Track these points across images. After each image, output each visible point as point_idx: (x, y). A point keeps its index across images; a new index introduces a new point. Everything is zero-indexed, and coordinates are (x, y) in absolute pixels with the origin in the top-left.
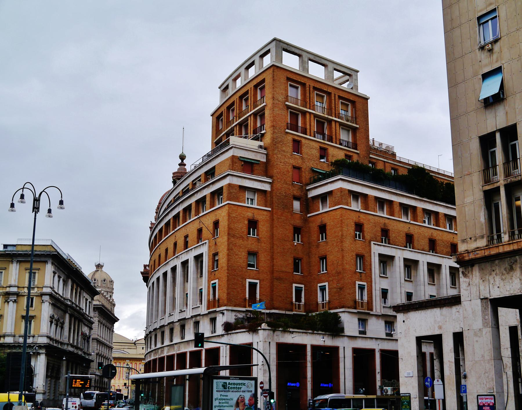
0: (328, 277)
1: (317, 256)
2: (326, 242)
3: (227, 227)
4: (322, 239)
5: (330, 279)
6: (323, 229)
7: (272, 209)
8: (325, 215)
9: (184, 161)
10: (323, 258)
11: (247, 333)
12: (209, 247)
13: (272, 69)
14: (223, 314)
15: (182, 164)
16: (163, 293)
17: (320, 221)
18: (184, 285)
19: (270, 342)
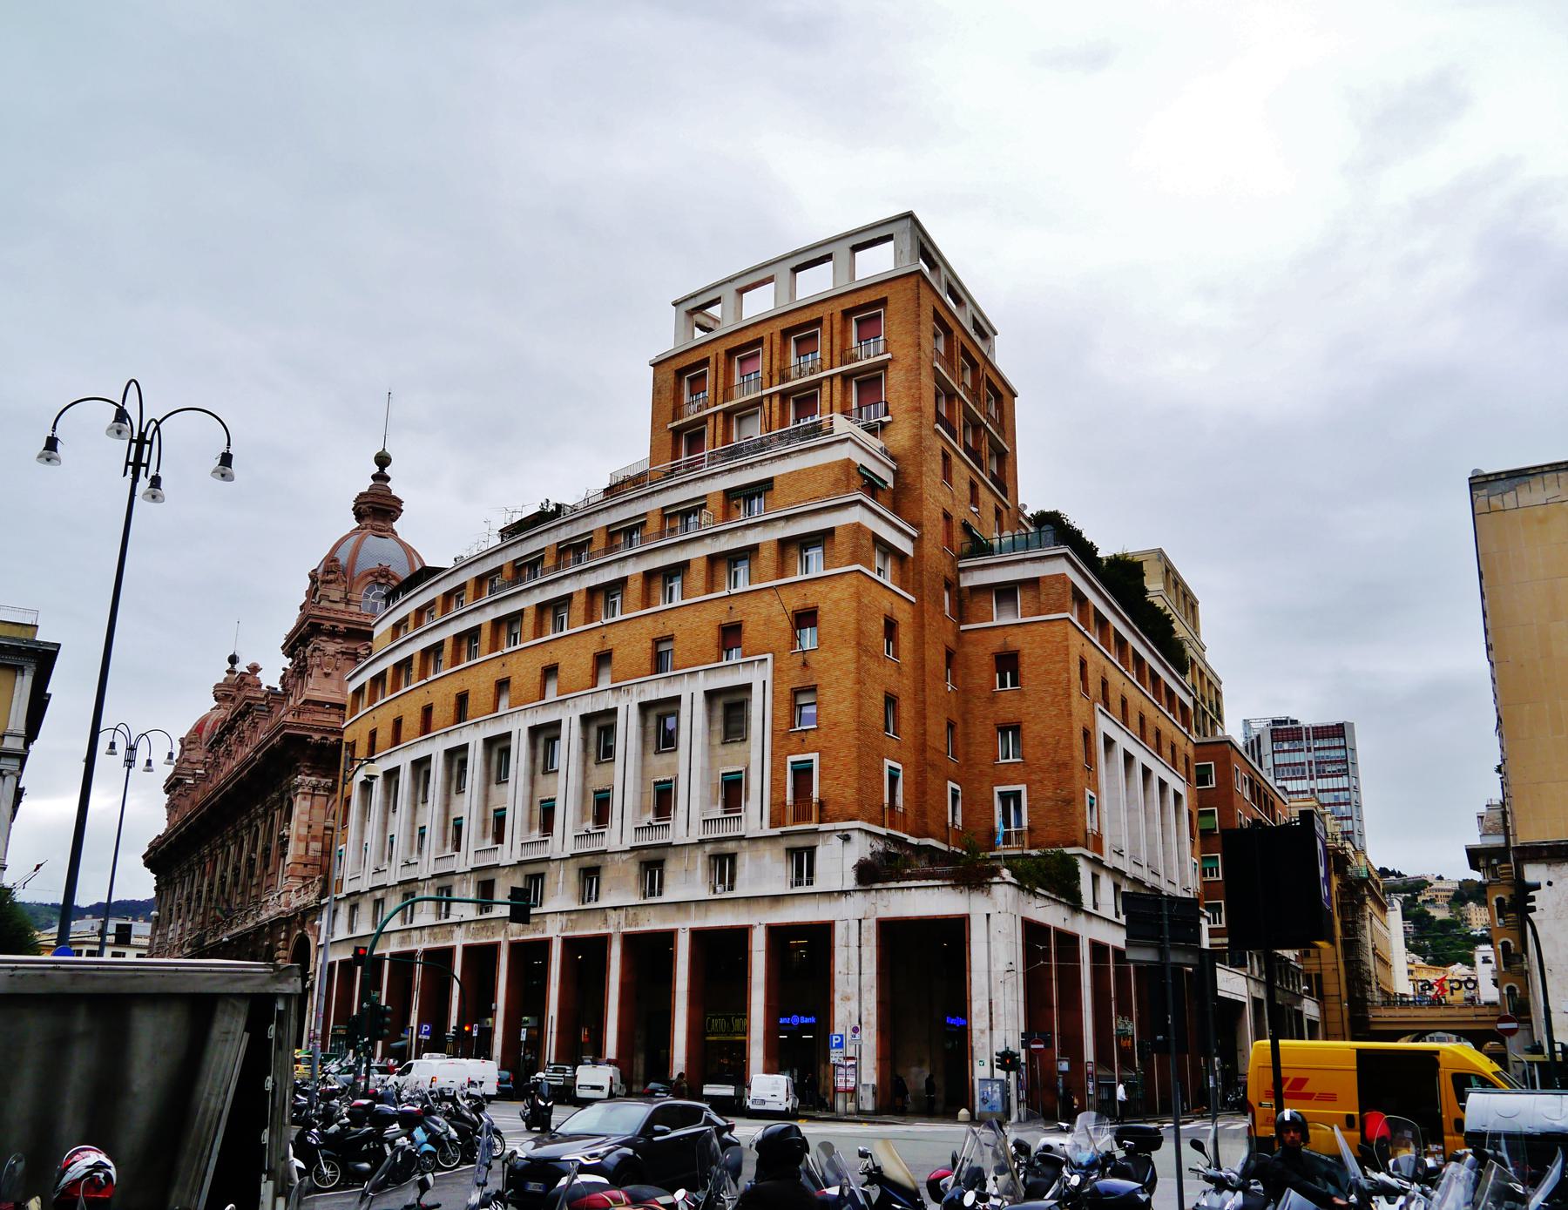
0: (1026, 770)
1: (990, 723)
2: (1022, 693)
4: (1003, 684)
5: (1033, 777)
7: (920, 598)
8: (1015, 630)
9: (387, 471)
10: (1013, 728)
12: (776, 670)
13: (913, 280)
14: (846, 839)
15: (381, 478)
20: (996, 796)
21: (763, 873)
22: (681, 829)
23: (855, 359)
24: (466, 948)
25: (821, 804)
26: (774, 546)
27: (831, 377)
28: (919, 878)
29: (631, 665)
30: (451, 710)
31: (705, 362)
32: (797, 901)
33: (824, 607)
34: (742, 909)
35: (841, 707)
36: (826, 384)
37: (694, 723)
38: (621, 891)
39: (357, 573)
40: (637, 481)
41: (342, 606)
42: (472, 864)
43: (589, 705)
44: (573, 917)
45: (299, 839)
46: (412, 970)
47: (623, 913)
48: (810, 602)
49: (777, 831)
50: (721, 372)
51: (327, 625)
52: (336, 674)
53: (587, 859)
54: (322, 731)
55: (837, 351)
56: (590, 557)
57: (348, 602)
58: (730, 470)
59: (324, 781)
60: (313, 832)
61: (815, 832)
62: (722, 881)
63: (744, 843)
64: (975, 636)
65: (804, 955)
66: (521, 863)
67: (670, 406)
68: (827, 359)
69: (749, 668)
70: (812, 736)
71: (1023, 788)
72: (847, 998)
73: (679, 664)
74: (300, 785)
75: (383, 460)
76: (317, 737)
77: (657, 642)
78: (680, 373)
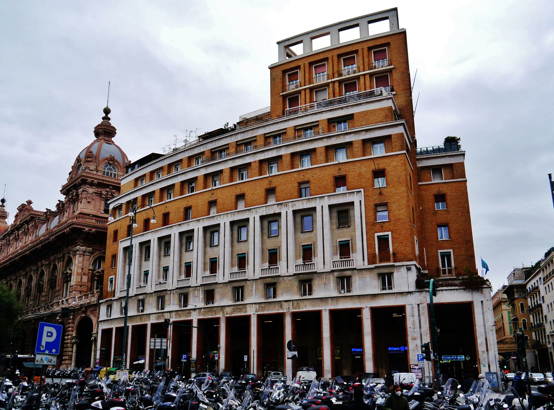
1: (434, 223)
3: (403, 177)
8: (443, 185)
9: (109, 116)
11: (462, 291)
14: (409, 269)
15: (106, 118)
19: (482, 302)
20: (439, 254)
21: (366, 284)
22: (221, 277)
23: (375, 67)
24: (199, 321)
25: (394, 253)
26: (361, 142)
27: (305, 89)
28: (446, 286)
29: (287, 194)
30: (182, 215)
31: (299, 67)
32: (385, 297)
33: (389, 169)
34: (357, 301)
35: (401, 212)
36: (303, 93)
37: (323, 219)
38: (224, 298)
39: (100, 159)
40: (259, 119)
41: (95, 172)
42: (154, 289)
43: (264, 212)
44: (263, 305)
45: (78, 274)
46: (217, 330)
47: (291, 303)
48: (381, 167)
49: (373, 266)
50: (307, 72)
51: (90, 180)
52: (93, 202)
53: (269, 279)
54: (89, 227)
55: (366, 64)
56: (287, 140)
57: (97, 171)
58: (330, 110)
59: (88, 249)
60: (84, 272)
61: (393, 266)
62: (343, 288)
63: (355, 272)
64: (425, 187)
65: (390, 322)
66: (230, 282)
67: (281, 85)
68: (361, 67)
69: (352, 195)
70: (386, 224)
71: (451, 251)
72: (414, 339)
73: (313, 193)
74: (78, 250)
75: (107, 111)
76: (87, 229)
77: (300, 184)
78: (284, 72)
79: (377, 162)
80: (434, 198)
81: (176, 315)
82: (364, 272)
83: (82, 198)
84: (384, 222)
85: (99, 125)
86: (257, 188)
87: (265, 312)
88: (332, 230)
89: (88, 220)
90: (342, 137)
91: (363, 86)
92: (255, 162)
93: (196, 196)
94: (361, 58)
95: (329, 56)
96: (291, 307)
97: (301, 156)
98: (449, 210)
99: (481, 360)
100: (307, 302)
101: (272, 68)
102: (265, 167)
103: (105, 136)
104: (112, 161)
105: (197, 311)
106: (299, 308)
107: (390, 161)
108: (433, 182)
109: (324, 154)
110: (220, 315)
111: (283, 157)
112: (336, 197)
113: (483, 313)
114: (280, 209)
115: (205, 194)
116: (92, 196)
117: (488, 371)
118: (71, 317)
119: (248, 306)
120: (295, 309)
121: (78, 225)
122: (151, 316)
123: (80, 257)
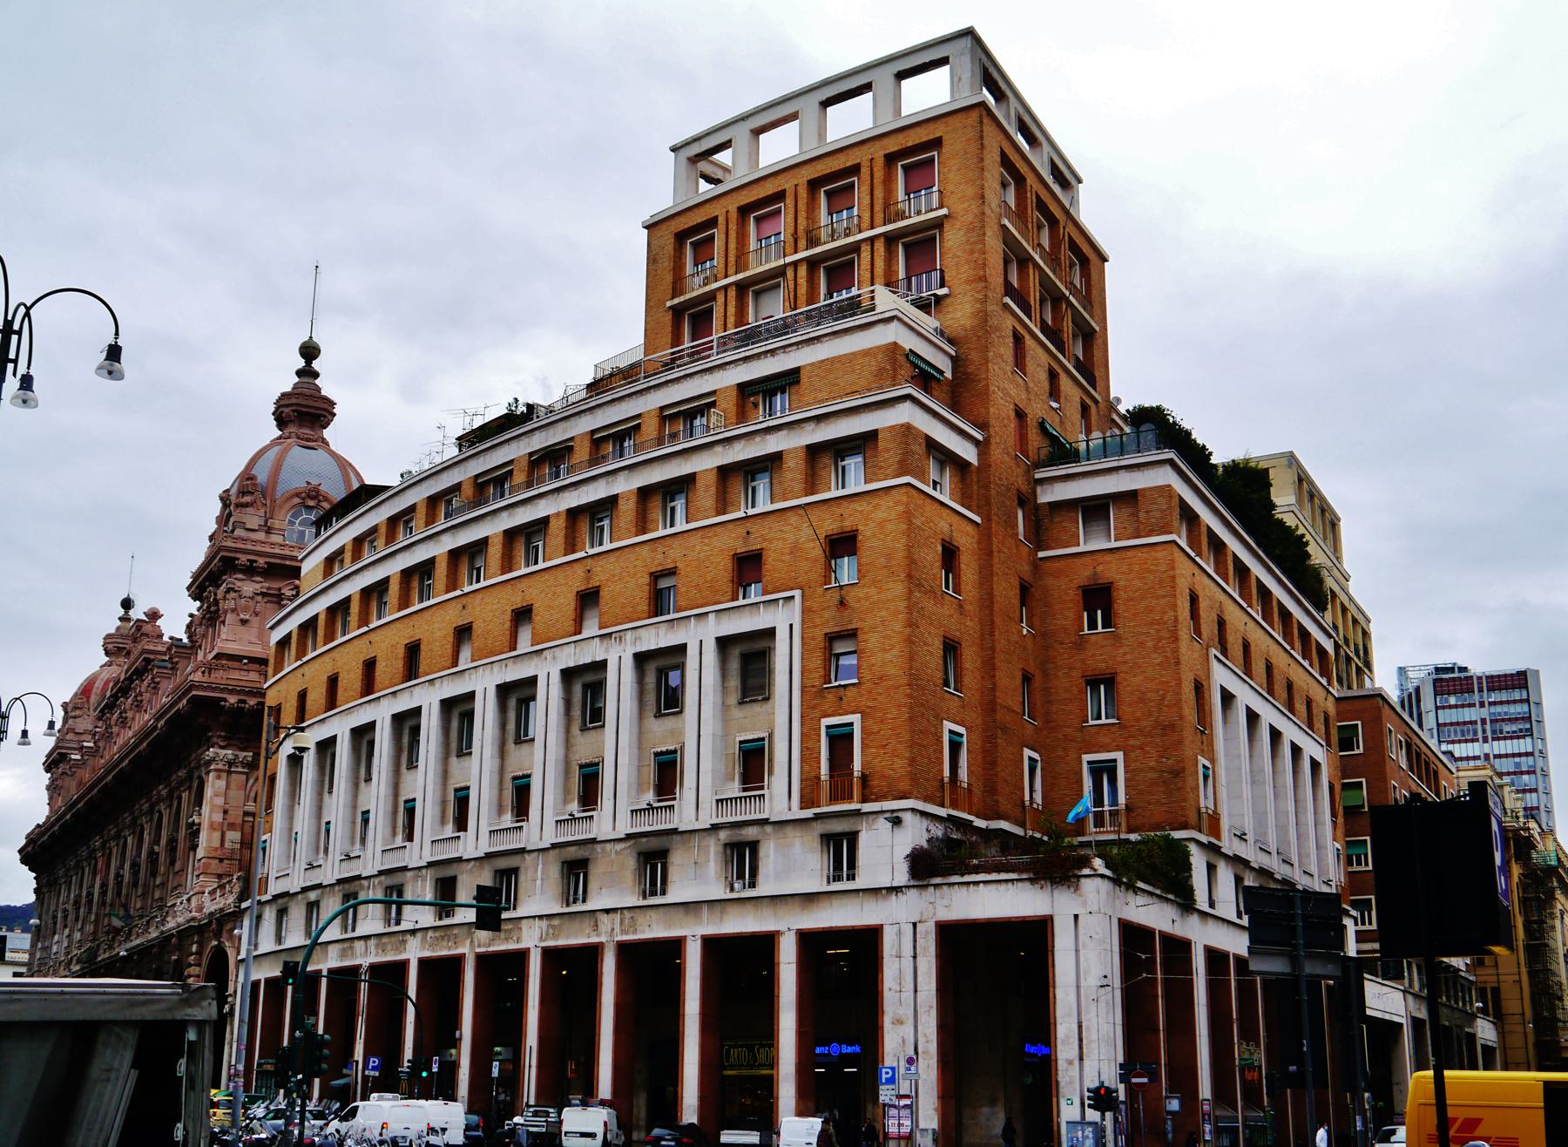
0: (1121, 735)
1: (1076, 674)
3: (900, 555)
5: (1132, 742)
6: (1098, 597)
7: (987, 518)
8: (1109, 557)
9: (316, 365)
11: (1027, 884)
12: (805, 611)
13: (975, 114)
14: (897, 822)
15: (308, 373)
16: (496, 749)
17: (1088, 573)
18: (640, 727)
19: (1076, 917)
20: (1085, 767)
21: (792, 865)
22: (687, 812)
24: (423, 962)
25: (864, 778)
26: (802, 454)
27: (872, 240)
30: (399, 664)
31: (713, 222)
32: (836, 902)
33: (866, 532)
35: (888, 656)
36: (866, 249)
37: (703, 677)
38: (612, 890)
39: (279, 494)
40: (628, 374)
41: (261, 536)
44: (556, 922)
45: (212, 827)
46: (678, 974)
47: (617, 917)
48: (848, 524)
49: (809, 813)
50: (733, 235)
51: (243, 559)
52: (255, 621)
53: (573, 849)
55: (878, 207)
57: (269, 531)
58: (746, 359)
59: (242, 754)
60: (231, 819)
62: (741, 876)
63: (768, 829)
66: (489, 856)
67: (669, 278)
68: (866, 216)
70: (851, 692)
71: (1119, 756)
75: (310, 351)
76: (233, 699)
77: (656, 576)
78: (681, 237)
79: (839, 511)
80: (1080, 598)
81: (377, 946)
82: (789, 830)
83: (226, 612)
84: (845, 686)
85: (284, 395)
86: (559, 589)
87: (562, 942)
88: (725, 707)
89: (235, 675)
90: (758, 439)
91: (868, 275)
92: (558, 514)
93: (430, 612)
94: (866, 188)
95: (787, 186)
96: (617, 930)
97: (746, 474)
98: (1121, 631)
99: (1062, 1084)
100: (653, 914)
101: (650, 227)
102: (736, 486)
103: (300, 426)
104: (312, 498)
105: (419, 935)
106: (635, 932)
107: (870, 508)
108: (1082, 548)
109: (713, 490)
110: (464, 949)
111: (621, 502)
112: (734, 616)
113: (1077, 951)
114: (607, 650)
115: (448, 605)
116: (251, 603)
117: (1078, 1118)
118: (194, 948)
119: (524, 923)
120: (627, 933)
121: (205, 689)
122: (331, 947)
123: (219, 777)
